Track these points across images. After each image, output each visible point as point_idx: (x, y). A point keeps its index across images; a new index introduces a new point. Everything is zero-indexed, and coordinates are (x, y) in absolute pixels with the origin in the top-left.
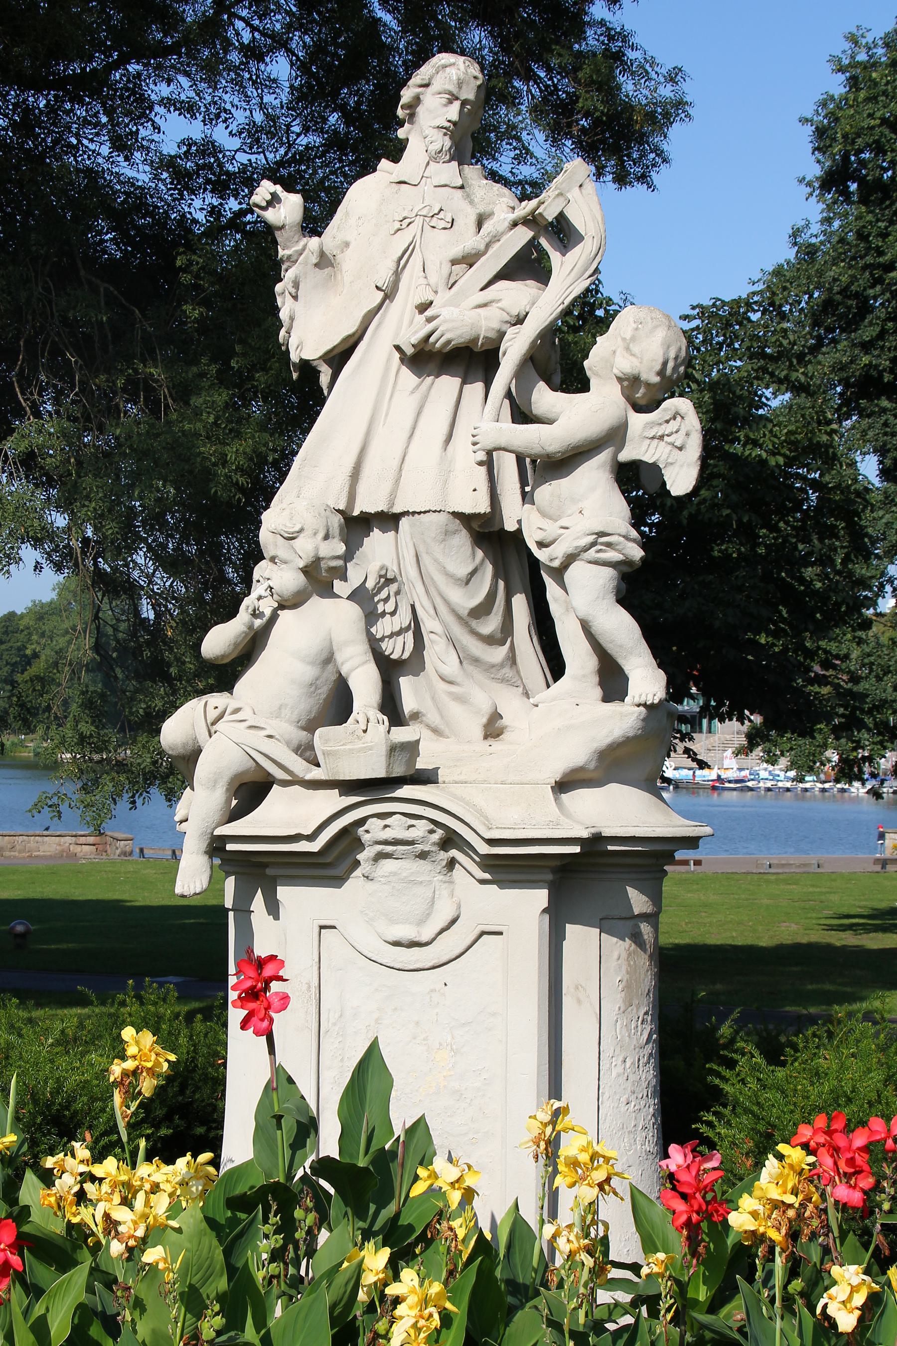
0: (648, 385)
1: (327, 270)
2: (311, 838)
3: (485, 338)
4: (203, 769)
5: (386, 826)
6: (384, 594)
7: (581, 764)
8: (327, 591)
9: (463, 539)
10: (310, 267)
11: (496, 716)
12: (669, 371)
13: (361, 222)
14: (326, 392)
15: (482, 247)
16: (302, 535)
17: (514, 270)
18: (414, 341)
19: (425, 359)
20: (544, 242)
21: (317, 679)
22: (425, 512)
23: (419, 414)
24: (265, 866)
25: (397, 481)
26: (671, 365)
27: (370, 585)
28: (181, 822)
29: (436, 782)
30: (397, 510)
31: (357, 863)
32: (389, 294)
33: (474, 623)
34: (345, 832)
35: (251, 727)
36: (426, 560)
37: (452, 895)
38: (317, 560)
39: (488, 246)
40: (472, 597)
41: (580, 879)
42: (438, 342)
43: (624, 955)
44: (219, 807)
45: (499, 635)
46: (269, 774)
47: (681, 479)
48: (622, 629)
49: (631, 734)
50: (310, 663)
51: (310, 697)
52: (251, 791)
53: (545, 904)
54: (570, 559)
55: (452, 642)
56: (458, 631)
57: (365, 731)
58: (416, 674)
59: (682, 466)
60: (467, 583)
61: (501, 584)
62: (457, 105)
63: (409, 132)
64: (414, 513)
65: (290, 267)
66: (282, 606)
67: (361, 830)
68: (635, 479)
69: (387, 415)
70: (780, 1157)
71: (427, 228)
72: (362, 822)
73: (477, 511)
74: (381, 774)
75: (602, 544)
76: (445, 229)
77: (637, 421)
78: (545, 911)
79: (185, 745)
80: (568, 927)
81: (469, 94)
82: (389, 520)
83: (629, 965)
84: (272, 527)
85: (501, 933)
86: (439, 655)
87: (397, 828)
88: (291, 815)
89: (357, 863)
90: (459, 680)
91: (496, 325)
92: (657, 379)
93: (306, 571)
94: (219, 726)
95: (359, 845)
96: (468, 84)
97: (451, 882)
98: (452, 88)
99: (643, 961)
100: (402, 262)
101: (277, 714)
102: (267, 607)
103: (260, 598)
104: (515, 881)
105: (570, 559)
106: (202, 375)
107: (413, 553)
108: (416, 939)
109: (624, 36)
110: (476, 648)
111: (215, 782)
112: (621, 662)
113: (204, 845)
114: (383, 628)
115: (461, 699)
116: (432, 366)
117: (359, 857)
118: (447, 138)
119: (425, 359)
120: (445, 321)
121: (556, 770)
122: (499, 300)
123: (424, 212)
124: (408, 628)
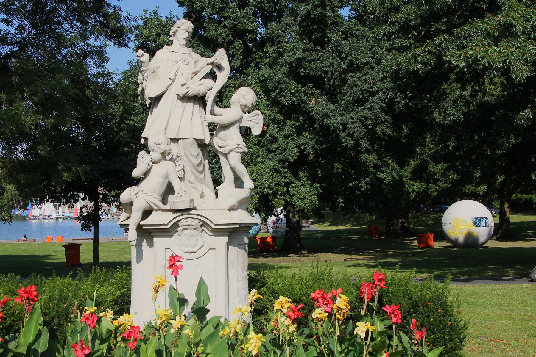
2: (166, 225)
6: (177, 160)
11: (203, 193)
19: (185, 98)
20: (215, 69)
24: (151, 233)
25: (179, 131)
36: (187, 151)
41: (233, 233)
42: (190, 94)
47: (257, 131)
48: (242, 169)
52: (147, 213)
54: (231, 151)
55: (193, 173)
68: (246, 132)
70: (341, 297)
77: (245, 116)
81: (191, 30)
87: (190, 222)
88: (158, 219)
98: (186, 28)
101: (154, 192)
105: (231, 151)
106: (17, 97)
109: (119, 8)
112: (242, 178)
116: (186, 100)
119: (185, 98)
121: (228, 206)
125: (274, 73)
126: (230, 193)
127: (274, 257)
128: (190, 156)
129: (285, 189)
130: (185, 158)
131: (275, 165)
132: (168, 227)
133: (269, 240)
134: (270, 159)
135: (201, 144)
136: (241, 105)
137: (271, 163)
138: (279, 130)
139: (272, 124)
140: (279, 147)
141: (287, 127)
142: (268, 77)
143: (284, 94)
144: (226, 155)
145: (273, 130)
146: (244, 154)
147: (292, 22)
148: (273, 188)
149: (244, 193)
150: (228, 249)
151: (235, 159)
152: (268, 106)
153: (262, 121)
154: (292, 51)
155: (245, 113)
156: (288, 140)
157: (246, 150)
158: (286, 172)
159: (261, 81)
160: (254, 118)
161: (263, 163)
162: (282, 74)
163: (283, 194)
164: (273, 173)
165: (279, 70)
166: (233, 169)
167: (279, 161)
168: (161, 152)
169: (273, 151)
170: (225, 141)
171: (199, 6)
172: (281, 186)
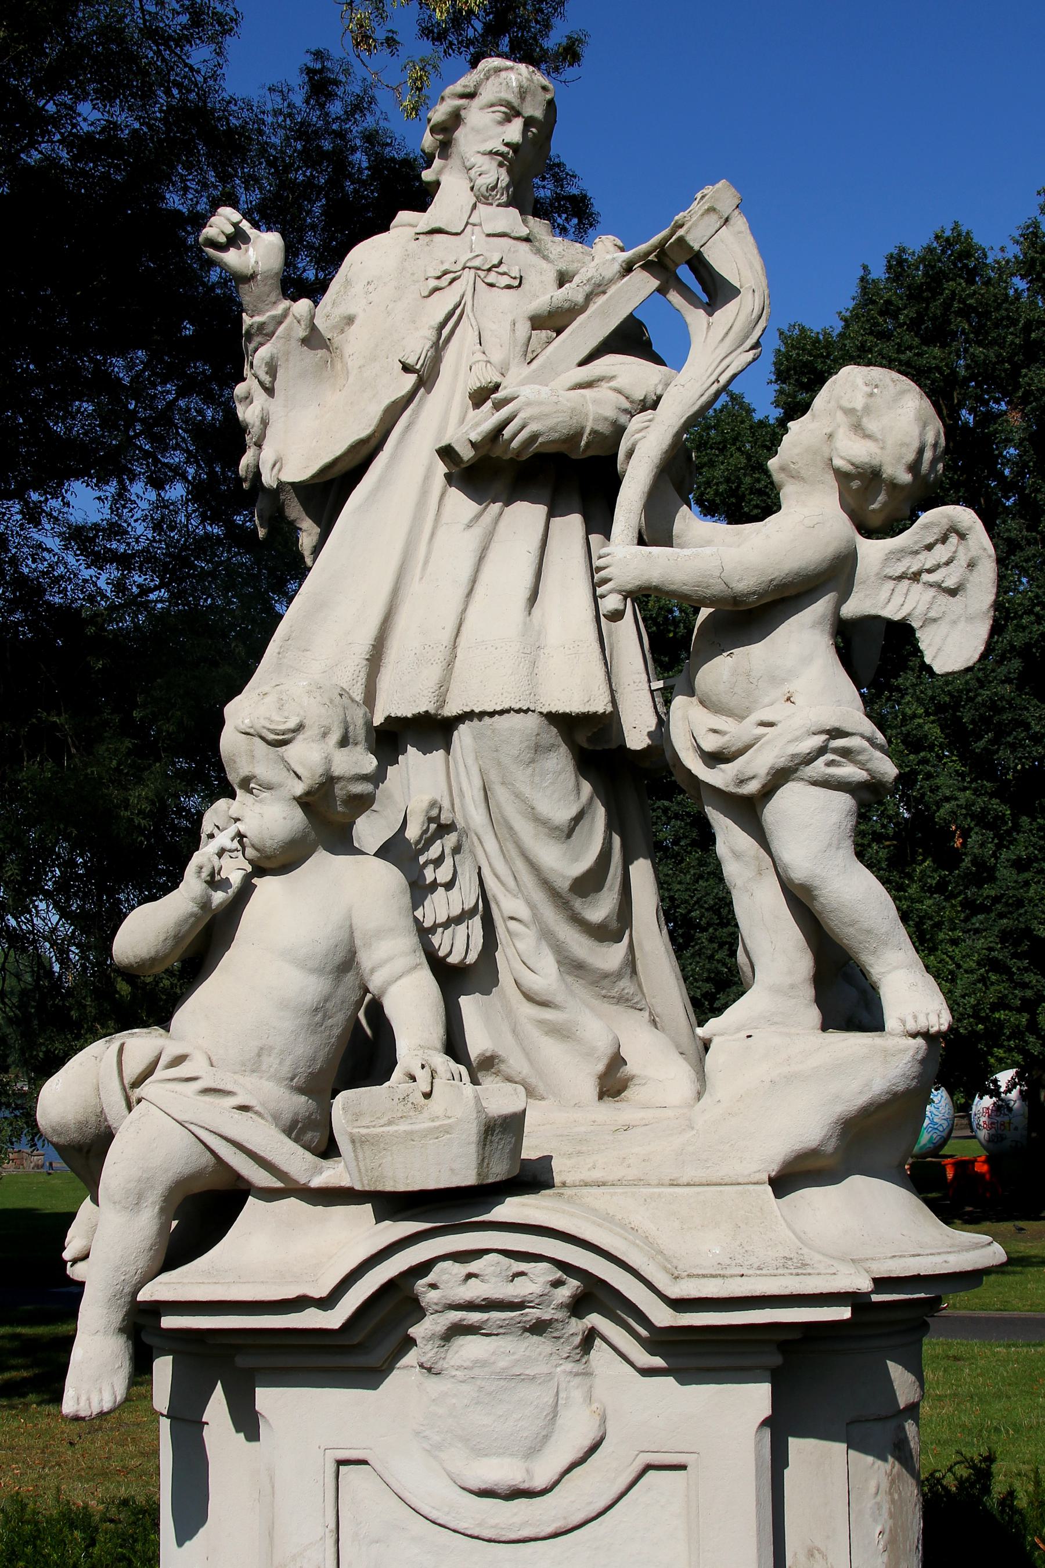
0: (894, 486)
1: (321, 353)
2: (327, 1303)
3: (594, 432)
4: (117, 1168)
5: (470, 1276)
6: (434, 852)
7: (813, 1144)
8: (342, 841)
9: (560, 762)
10: (295, 344)
11: (617, 1061)
12: (925, 466)
13: (371, 288)
14: (308, 561)
15: (580, 298)
16: (300, 737)
17: (630, 338)
18: (475, 436)
21: (326, 1000)
22: (502, 712)
23: (481, 559)
26: (928, 455)
27: (412, 833)
28: (75, 1261)
29: (549, 1184)
30: (451, 710)
31: (410, 1342)
32: (425, 377)
33: (578, 904)
34: (389, 1287)
35: (207, 1091)
36: (501, 794)
37: (589, 1398)
38: (329, 781)
39: (589, 298)
40: (576, 859)
42: (516, 438)
43: (885, 1484)
44: (147, 1244)
45: (614, 925)
46: (239, 1177)
47: (954, 642)
48: (860, 898)
49: (901, 1088)
50: (313, 971)
51: (314, 1032)
52: (203, 1210)
53: (766, 1411)
54: (780, 777)
55: (546, 935)
56: (551, 915)
57: (427, 1095)
58: (487, 992)
59: (954, 622)
60: (569, 835)
61: (617, 840)
62: (518, 124)
63: (440, 172)
64: (482, 715)
65: (262, 344)
66: (259, 870)
67: (421, 1284)
68: (879, 655)
69: (426, 562)
71: (480, 285)
72: (423, 1268)
73: (592, 709)
74: (467, 1177)
75: (835, 751)
76: (509, 287)
77: (872, 552)
78: (765, 1423)
79: (82, 1125)
80: (790, 1439)
82: (433, 730)
83: (893, 1501)
84: (246, 723)
85: (683, 1467)
86: (528, 957)
87: (492, 1280)
88: (285, 1257)
89: (410, 1342)
90: (559, 999)
91: (610, 413)
92: (906, 478)
93: (307, 802)
94: (147, 1089)
95: (416, 1310)
96: (534, 95)
97: (588, 1374)
98: (512, 98)
99: (911, 1491)
100: (445, 332)
101: (254, 1065)
102: (234, 872)
103: (221, 853)
104: (708, 1370)
105: (780, 777)
107: (477, 783)
108: (525, 1486)
110: (580, 946)
111: (140, 1197)
113: (117, 1317)
114: (438, 907)
115: (560, 1032)
117: (413, 1331)
118: (503, 171)
119: (492, 471)
120: (529, 404)
121: (773, 1151)
122: (612, 378)
123: (476, 263)
124: (473, 912)
125: (978, 680)
126: (784, 1068)
127: (999, 1220)
128: (525, 830)
129: (1024, 1018)
130: (491, 844)
131: (991, 949)
132: (334, 1319)
133: (981, 1168)
134: (977, 931)
135: (589, 741)
136: (842, 477)
137: (980, 943)
138: (999, 846)
139: (976, 829)
140: (1002, 895)
141: (1021, 837)
142: (960, 691)
143: (1010, 739)
144: (749, 810)
145: (982, 845)
146: (867, 795)
147: (1025, 533)
148: (987, 1017)
149: (874, 1066)
150: (779, 1460)
151: (812, 829)
152: (962, 775)
153: (987, 572)
154: (1030, 612)
155: (869, 532)
156: (1027, 875)
157: (888, 769)
158: (1026, 970)
159: (941, 708)
160: (929, 559)
161: (954, 942)
162: (1003, 682)
163: (1017, 1033)
164: (987, 972)
165: (993, 671)
166: (801, 901)
167: (1004, 936)
168: (299, 789)
169: (987, 910)
170: (740, 716)
171: (756, 506)
172: (1011, 1009)
